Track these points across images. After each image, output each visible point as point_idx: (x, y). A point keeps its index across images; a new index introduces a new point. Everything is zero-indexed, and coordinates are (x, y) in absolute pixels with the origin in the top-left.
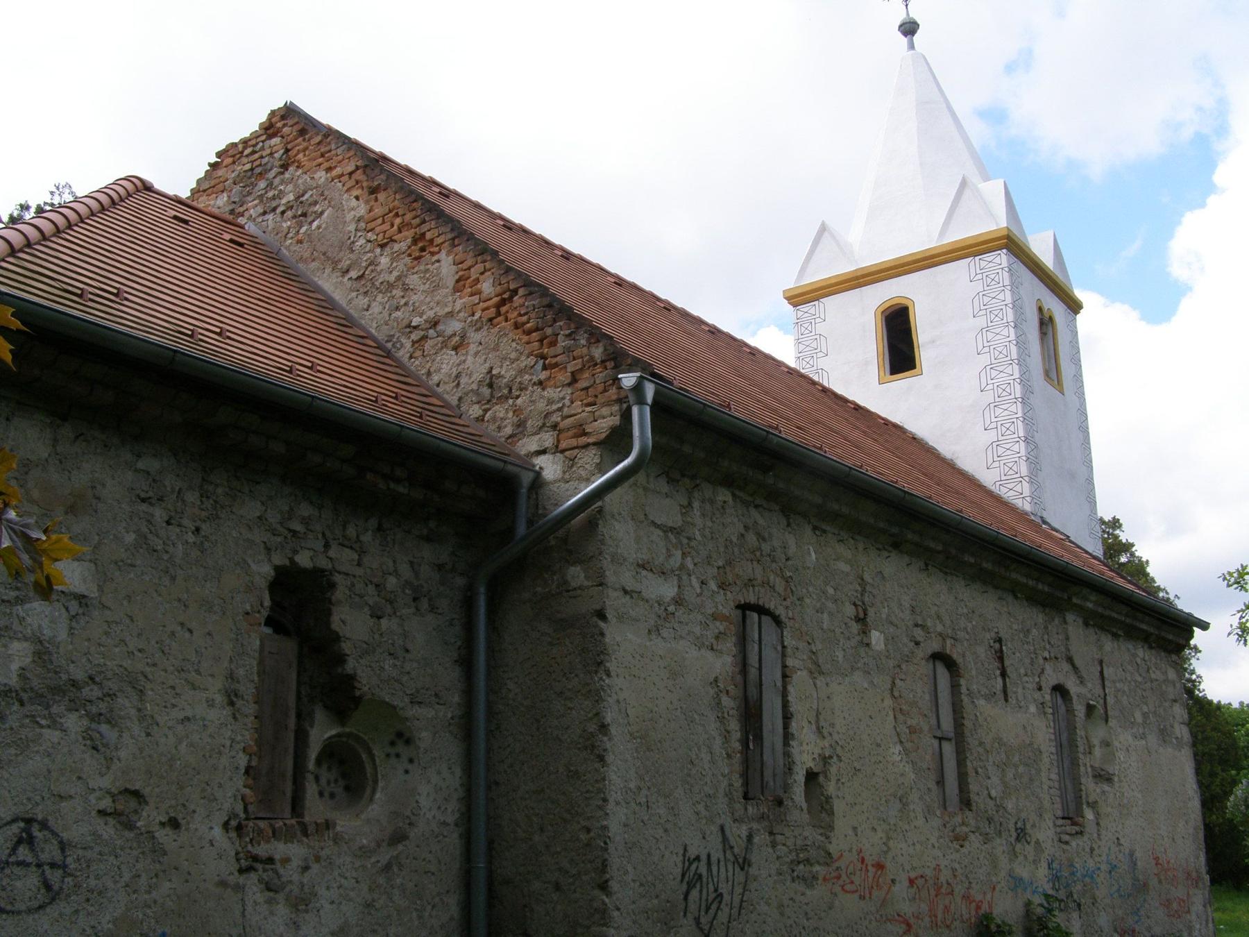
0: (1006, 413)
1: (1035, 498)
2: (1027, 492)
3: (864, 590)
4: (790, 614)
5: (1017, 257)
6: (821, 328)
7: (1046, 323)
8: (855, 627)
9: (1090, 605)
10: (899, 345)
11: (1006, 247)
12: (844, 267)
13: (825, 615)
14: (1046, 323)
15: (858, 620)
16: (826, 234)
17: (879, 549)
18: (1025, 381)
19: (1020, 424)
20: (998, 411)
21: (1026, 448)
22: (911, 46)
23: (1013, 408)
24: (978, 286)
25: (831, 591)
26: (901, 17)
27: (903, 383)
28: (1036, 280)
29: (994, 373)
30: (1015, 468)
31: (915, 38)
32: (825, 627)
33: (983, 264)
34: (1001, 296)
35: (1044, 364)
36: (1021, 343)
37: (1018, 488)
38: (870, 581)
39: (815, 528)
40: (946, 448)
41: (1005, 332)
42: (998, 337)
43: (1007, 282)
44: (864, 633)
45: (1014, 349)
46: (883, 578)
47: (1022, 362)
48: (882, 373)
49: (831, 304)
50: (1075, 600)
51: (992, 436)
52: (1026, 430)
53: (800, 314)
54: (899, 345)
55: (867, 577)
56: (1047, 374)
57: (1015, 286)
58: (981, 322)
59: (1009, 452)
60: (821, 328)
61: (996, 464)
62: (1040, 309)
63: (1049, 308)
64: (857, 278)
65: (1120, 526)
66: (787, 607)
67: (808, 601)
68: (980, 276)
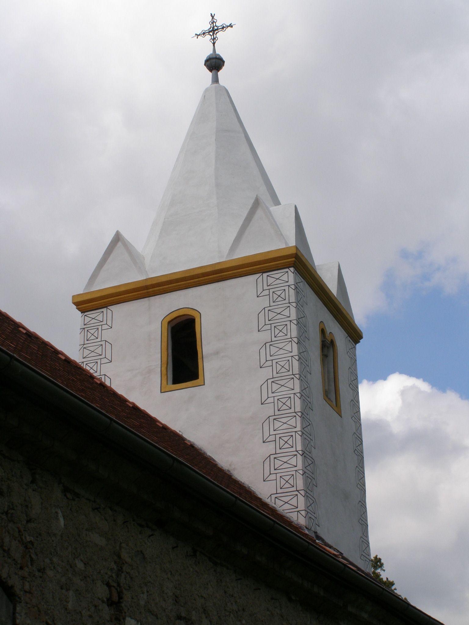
0: (285, 426)
1: (310, 512)
2: (302, 505)
3: (120, 570)
4: (27, 587)
5: (304, 278)
6: (107, 335)
7: (327, 346)
8: (106, 612)
9: (365, 616)
10: (183, 354)
11: (294, 265)
12: (134, 277)
13: (71, 593)
14: (327, 346)
15: (110, 603)
16: (120, 244)
17: (141, 526)
18: (305, 396)
19: (299, 438)
20: (277, 424)
21: (304, 462)
22: (216, 80)
23: (292, 422)
24: (265, 302)
25: (80, 565)
26: (208, 52)
27: (184, 393)
28: (320, 304)
29: (275, 387)
30: (291, 481)
31: (220, 73)
32: (70, 606)
33: (271, 280)
34: (286, 313)
35: (324, 386)
36: (302, 358)
37: (294, 502)
38: (129, 560)
39: (66, 490)
40: (223, 459)
41: (288, 348)
42: (281, 352)
43: (293, 299)
44: (117, 619)
45: (296, 364)
46: (144, 558)
47: (303, 377)
48: (164, 382)
49: (119, 311)
50: (350, 609)
51: (270, 448)
52: (303, 444)
53: (87, 319)
54: (183, 354)
55: (125, 555)
56: (326, 394)
57: (300, 305)
58: (265, 336)
59: (286, 465)
60: (107, 335)
61: (273, 477)
62: (323, 331)
63: (330, 340)
64: (146, 287)
65: (382, 565)
66: (24, 578)
67: (50, 573)
68: (266, 292)
